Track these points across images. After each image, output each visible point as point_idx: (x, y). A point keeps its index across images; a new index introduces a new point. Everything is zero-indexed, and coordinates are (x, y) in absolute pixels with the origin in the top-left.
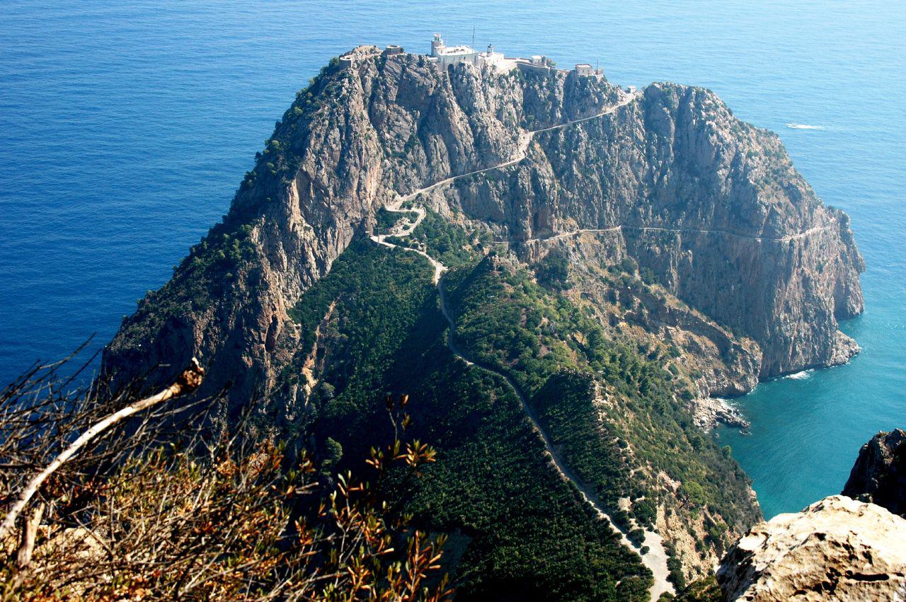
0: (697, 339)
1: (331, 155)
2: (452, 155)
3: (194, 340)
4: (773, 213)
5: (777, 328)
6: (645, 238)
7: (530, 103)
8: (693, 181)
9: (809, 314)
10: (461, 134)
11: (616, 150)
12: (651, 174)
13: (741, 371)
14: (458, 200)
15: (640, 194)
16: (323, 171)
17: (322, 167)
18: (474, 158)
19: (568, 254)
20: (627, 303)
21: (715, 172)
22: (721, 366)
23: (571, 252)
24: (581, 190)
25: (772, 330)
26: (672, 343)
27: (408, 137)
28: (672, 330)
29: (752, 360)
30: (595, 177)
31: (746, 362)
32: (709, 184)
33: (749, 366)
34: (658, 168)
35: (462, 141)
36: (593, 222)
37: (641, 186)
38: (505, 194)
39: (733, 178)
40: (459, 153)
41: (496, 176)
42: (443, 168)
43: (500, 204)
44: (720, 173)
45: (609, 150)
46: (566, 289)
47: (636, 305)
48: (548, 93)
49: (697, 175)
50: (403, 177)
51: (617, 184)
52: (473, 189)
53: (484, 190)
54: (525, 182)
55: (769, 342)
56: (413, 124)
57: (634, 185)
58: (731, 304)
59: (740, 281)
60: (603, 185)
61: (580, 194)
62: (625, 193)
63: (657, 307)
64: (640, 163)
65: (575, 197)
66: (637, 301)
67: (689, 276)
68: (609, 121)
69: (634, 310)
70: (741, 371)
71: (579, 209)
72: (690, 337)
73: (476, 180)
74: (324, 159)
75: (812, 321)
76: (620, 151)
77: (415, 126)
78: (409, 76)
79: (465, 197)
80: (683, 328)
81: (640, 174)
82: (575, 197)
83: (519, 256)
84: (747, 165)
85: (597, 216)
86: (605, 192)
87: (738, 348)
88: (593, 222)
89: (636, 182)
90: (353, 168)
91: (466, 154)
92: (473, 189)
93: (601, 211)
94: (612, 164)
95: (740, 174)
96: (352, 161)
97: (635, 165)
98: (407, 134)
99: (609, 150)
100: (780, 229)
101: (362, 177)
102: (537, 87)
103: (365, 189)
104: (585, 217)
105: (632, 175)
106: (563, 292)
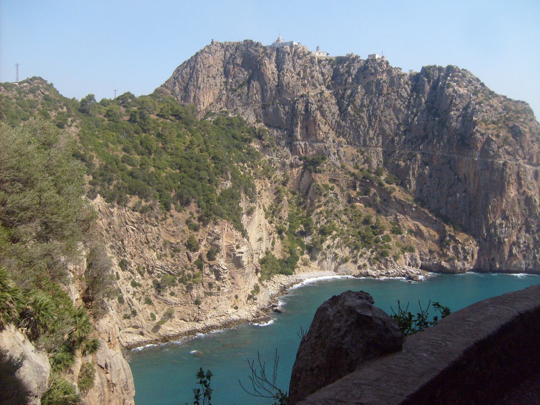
0: (422, 228)
1: (182, 80)
2: (263, 91)
3: (353, 278)
4: (489, 141)
5: (493, 230)
6: (397, 156)
7: (336, 75)
8: (434, 120)
9: (530, 227)
10: (270, 80)
11: (382, 100)
12: (407, 116)
13: (450, 253)
14: (262, 116)
15: (398, 128)
16: (177, 87)
17: (176, 85)
18: (274, 92)
19: (329, 155)
20: (366, 192)
21: (449, 113)
22: (435, 247)
23: (332, 154)
24: (352, 121)
25: (488, 230)
26: (399, 225)
27: (242, 82)
28: (400, 216)
29: (463, 249)
30: (364, 115)
31: (458, 249)
32: (444, 123)
33: (459, 252)
34: (412, 113)
35: (269, 83)
36: (359, 143)
37: (400, 124)
38: (288, 112)
39: (463, 117)
40: (266, 90)
41: (284, 103)
42: (256, 98)
43: (284, 118)
44: (452, 113)
45: (378, 100)
46: (316, 172)
47: (371, 194)
48: (346, 69)
49: (439, 116)
50: (231, 101)
51: (380, 121)
52: (271, 110)
53: (276, 111)
54: (300, 107)
55: (486, 240)
56: (247, 76)
57: (394, 123)
58: (457, 208)
59: (465, 191)
60: (370, 121)
61: (351, 124)
62: (386, 127)
63: (386, 196)
64: (400, 110)
65: (347, 125)
66: (373, 190)
67: (425, 184)
68: (380, 83)
69: (369, 196)
70: (450, 253)
71: (350, 133)
72: (418, 227)
73: (273, 104)
74: (178, 81)
75: (533, 233)
76: (385, 101)
77: (248, 77)
78: (248, 51)
79: (266, 114)
80: (413, 218)
81: (400, 117)
82: (347, 125)
83: (291, 150)
84: (475, 108)
85: (362, 139)
86: (370, 124)
87: (452, 238)
88: (359, 143)
89: (396, 121)
90: (192, 87)
91: (270, 91)
92: (271, 110)
93: (365, 136)
94: (378, 108)
95: (468, 115)
96: (192, 83)
97: (397, 111)
98: (242, 80)
99: (378, 100)
100: (493, 152)
101: (197, 92)
102: (340, 67)
103: (198, 99)
104: (353, 139)
105: (394, 117)
106: (313, 174)
